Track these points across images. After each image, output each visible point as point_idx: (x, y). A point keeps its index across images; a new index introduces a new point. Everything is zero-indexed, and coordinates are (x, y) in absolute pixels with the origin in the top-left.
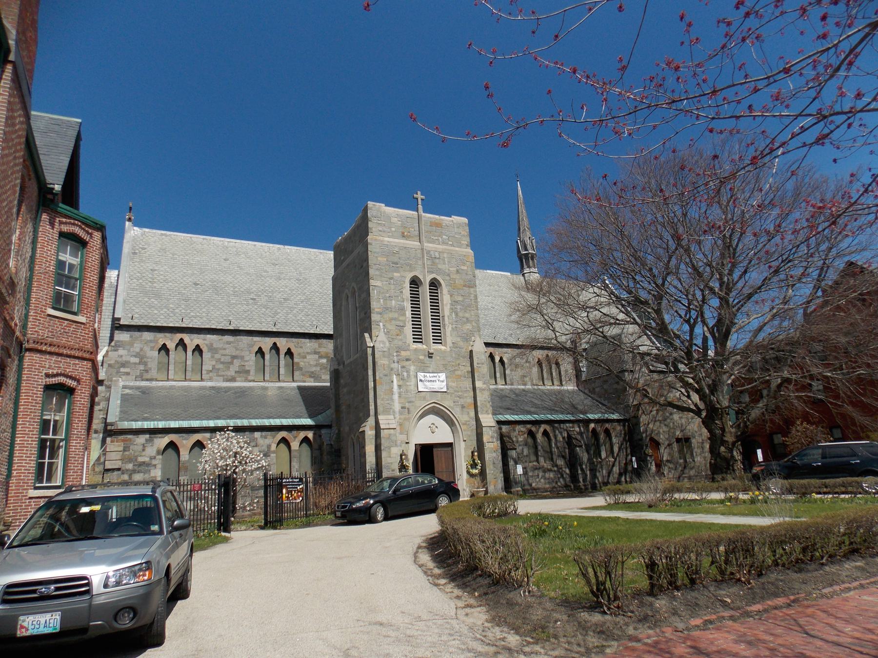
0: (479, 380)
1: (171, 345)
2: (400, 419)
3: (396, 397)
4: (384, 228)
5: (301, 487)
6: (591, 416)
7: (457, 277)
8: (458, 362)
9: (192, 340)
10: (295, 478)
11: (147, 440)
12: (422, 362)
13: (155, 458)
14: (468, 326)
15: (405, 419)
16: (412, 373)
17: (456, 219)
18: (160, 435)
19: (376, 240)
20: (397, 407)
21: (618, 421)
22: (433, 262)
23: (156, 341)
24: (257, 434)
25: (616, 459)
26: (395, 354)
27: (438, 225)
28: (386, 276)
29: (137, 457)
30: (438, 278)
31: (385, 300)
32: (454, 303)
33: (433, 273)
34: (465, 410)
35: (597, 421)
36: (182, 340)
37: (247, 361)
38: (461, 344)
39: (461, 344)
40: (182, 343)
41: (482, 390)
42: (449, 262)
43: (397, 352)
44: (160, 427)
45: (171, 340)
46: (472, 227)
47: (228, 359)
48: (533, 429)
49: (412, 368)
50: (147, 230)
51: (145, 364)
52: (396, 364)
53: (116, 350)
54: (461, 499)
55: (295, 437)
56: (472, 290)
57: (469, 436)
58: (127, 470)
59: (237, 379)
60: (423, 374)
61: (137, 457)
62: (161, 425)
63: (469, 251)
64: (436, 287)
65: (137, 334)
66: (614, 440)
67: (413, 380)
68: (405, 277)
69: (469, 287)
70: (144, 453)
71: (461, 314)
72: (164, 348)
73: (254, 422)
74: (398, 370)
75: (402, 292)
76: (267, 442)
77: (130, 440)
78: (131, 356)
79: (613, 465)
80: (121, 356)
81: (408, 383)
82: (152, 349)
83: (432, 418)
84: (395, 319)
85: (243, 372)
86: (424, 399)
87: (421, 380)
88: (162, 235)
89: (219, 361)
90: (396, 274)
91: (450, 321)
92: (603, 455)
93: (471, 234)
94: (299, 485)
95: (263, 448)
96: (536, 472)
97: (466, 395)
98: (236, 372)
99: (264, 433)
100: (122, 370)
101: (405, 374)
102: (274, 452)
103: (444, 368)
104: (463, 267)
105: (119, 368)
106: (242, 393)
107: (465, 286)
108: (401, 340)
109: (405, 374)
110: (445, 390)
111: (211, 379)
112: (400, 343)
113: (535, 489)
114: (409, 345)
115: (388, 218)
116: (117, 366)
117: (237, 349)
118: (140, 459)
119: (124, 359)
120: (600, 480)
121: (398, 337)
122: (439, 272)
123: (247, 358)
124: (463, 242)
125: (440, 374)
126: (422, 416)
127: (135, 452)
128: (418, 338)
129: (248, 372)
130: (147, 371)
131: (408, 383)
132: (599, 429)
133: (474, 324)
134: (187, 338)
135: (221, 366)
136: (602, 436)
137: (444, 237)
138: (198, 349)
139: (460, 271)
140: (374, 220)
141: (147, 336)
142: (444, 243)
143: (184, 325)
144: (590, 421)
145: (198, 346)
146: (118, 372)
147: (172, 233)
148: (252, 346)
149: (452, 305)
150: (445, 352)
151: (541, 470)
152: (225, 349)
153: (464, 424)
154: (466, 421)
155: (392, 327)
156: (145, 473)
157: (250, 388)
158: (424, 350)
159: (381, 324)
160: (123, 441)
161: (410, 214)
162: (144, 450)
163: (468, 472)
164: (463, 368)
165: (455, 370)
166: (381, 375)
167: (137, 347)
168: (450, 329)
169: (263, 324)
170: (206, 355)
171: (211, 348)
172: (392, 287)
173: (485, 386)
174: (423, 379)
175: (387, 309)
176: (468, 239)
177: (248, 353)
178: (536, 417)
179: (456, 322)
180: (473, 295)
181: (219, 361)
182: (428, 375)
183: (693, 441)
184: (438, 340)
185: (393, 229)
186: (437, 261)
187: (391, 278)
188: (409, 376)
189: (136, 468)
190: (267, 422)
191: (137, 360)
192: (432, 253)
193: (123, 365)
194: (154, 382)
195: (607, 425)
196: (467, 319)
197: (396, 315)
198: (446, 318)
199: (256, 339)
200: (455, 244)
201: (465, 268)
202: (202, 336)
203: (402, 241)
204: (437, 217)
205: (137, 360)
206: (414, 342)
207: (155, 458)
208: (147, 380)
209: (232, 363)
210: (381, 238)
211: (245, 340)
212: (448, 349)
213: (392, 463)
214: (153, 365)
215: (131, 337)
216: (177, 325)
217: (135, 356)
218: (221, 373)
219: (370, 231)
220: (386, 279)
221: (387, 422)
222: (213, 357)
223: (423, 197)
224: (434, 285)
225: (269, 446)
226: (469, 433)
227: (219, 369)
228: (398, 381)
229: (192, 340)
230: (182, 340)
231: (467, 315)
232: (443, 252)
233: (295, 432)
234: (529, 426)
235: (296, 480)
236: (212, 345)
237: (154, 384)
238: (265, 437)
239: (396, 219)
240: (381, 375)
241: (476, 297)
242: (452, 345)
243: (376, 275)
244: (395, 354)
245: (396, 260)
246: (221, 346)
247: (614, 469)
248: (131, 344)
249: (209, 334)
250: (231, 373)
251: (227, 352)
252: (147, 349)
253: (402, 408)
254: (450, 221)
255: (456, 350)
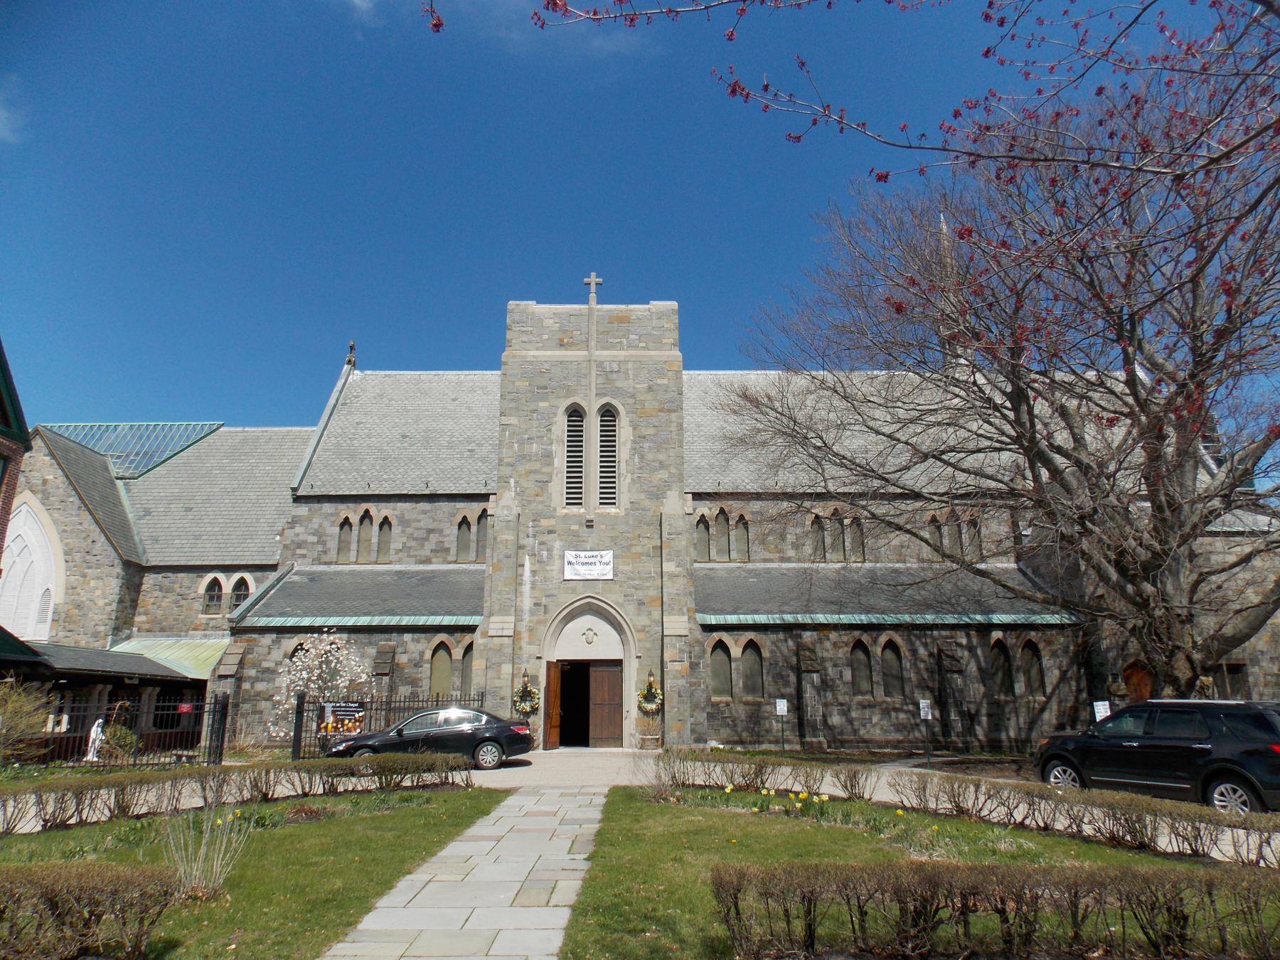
0: (668, 560)
1: (355, 519)
2: (530, 621)
3: (526, 588)
4: (531, 337)
5: (361, 714)
6: (997, 618)
7: (649, 397)
8: (637, 533)
9: (379, 511)
10: (352, 702)
11: (273, 641)
12: (575, 534)
13: (281, 663)
14: (663, 475)
15: (539, 622)
16: (556, 552)
17: (656, 305)
18: (288, 635)
19: (514, 356)
20: (527, 602)
21: (1061, 627)
22: (608, 379)
23: (337, 514)
24: (407, 637)
25: (1049, 698)
26: (530, 524)
27: (624, 319)
28: (525, 408)
29: (261, 661)
30: (615, 402)
31: (521, 443)
32: (639, 439)
33: (605, 395)
34: (643, 608)
35: (1004, 627)
36: (367, 512)
37: (446, 536)
38: (647, 503)
39: (647, 503)
40: (366, 515)
41: (673, 576)
42: (635, 376)
43: (534, 521)
44: (374, 624)
45: (355, 512)
46: (681, 312)
47: (422, 534)
48: (865, 638)
49: (558, 544)
50: (369, 372)
51: (324, 543)
52: (531, 539)
53: (292, 528)
54: (223, 763)
55: (458, 642)
56: (674, 416)
57: (649, 650)
58: (249, 677)
59: (434, 560)
60: (573, 553)
61: (261, 661)
62: (291, 622)
63: (677, 353)
64: (614, 416)
65: (316, 506)
66: (1046, 662)
67: (557, 562)
68: (557, 407)
69: (669, 411)
70: (269, 657)
71: (650, 456)
72: (346, 522)
73: (406, 620)
74: (534, 548)
75: (550, 430)
76: (420, 647)
77: (255, 640)
78: (309, 534)
79: (1043, 710)
80: (298, 535)
81: (548, 568)
82: (333, 524)
83: (588, 621)
84: (535, 472)
85: (441, 550)
86: (574, 590)
87: (570, 563)
88: (386, 375)
89: (411, 537)
90: (542, 404)
91: (630, 468)
92: (1019, 688)
93: (682, 328)
94: (358, 712)
95: (414, 655)
96: (867, 712)
97: (647, 584)
98: (432, 551)
99: (416, 636)
100: (298, 551)
101: (545, 553)
102: (427, 662)
103: (613, 543)
104: (659, 382)
105: (295, 549)
106: (428, 578)
107: (661, 410)
108: (542, 502)
109: (545, 553)
110: (610, 577)
111: (400, 561)
112: (541, 507)
113: (865, 741)
114: (555, 510)
115: (539, 320)
116: (292, 547)
117: (434, 520)
118: (265, 665)
119: (301, 538)
120: (1012, 734)
121: (540, 499)
122: (617, 392)
123: (446, 532)
124: (665, 341)
125: (603, 553)
126: (571, 617)
127: (259, 655)
128: (574, 497)
129: (447, 550)
130: (325, 552)
131: (548, 568)
132: (1011, 640)
133: (673, 470)
134: (373, 508)
135: (413, 544)
136: (1018, 655)
137: (632, 337)
138: (386, 522)
139: (654, 388)
140: (516, 328)
141: (328, 507)
142: (630, 347)
143: (369, 492)
144: (991, 627)
145: (386, 518)
146: (294, 554)
147: (398, 372)
148: (454, 515)
149: (634, 442)
150: (616, 517)
151: (877, 710)
152: (419, 521)
153: (639, 631)
154: (644, 626)
155: (529, 484)
156: (268, 682)
157: (325, 573)
158: (580, 516)
159: (512, 481)
160: (247, 641)
161: (575, 310)
162: (269, 653)
163: (640, 708)
164: (645, 541)
165: (632, 545)
166: (501, 557)
167: (316, 522)
168: (628, 480)
169: (472, 485)
170: (396, 529)
171: (404, 522)
172: (535, 423)
173: (680, 569)
174: (573, 560)
175: (523, 457)
176: (676, 335)
177: (448, 524)
178: (874, 618)
179: (641, 468)
180: (674, 424)
181: (411, 537)
182: (582, 554)
183: (1253, 670)
184: (608, 497)
185: (546, 337)
186: (615, 376)
187: (534, 411)
188: (550, 556)
189: (259, 675)
190: (421, 620)
191: (314, 539)
192: (607, 365)
193: (300, 545)
194: (333, 567)
195: (1033, 635)
196: (661, 463)
197: (536, 466)
198: (623, 465)
199: (460, 505)
200: (651, 345)
201: (665, 381)
202: (391, 505)
203: (557, 353)
204: (623, 307)
205: (314, 539)
206: (601, 504)
207: (281, 663)
208: (325, 563)
209: (427, 539)
210: (524, 353)
211: (445, 506)
212: (623, 513)
213: (501, 688)
214: (333, 544)
215: (310, 510)
216: (361, 492)
217: (313, 534)
218: (412, 553)
219: (507, 344)
220: (525, 413)
221: (501, 626)
222: (403, 532)
223: (599, 280)
224: (608, 413)
225: (422, 653)
226: (648, 645)
227: (410, 548)
228: (532, 564)
229: (379, 511)
230: (367, 512)
231: (661, 457)
232: (626, 362)
233: (458, 635)
234: (857, 633)
235: (353, 705)
236: (403, 515)
237: (333, 568)
238: (418, 641)
239: (552, 321)
240: (501, 557)
241: (680, 427)
242: (629, 506)
243: (511, 408)
244: (530, 524)
245: (544, 382)
246: (414, 517)
247: (1046, 715)
248: (309, 520)
249: (400, 501)
250: (426, 552)
251: (422, 524)
252: (327, 524)
253: (536, 604)
254: (645, 310)
255: (637, 513)
